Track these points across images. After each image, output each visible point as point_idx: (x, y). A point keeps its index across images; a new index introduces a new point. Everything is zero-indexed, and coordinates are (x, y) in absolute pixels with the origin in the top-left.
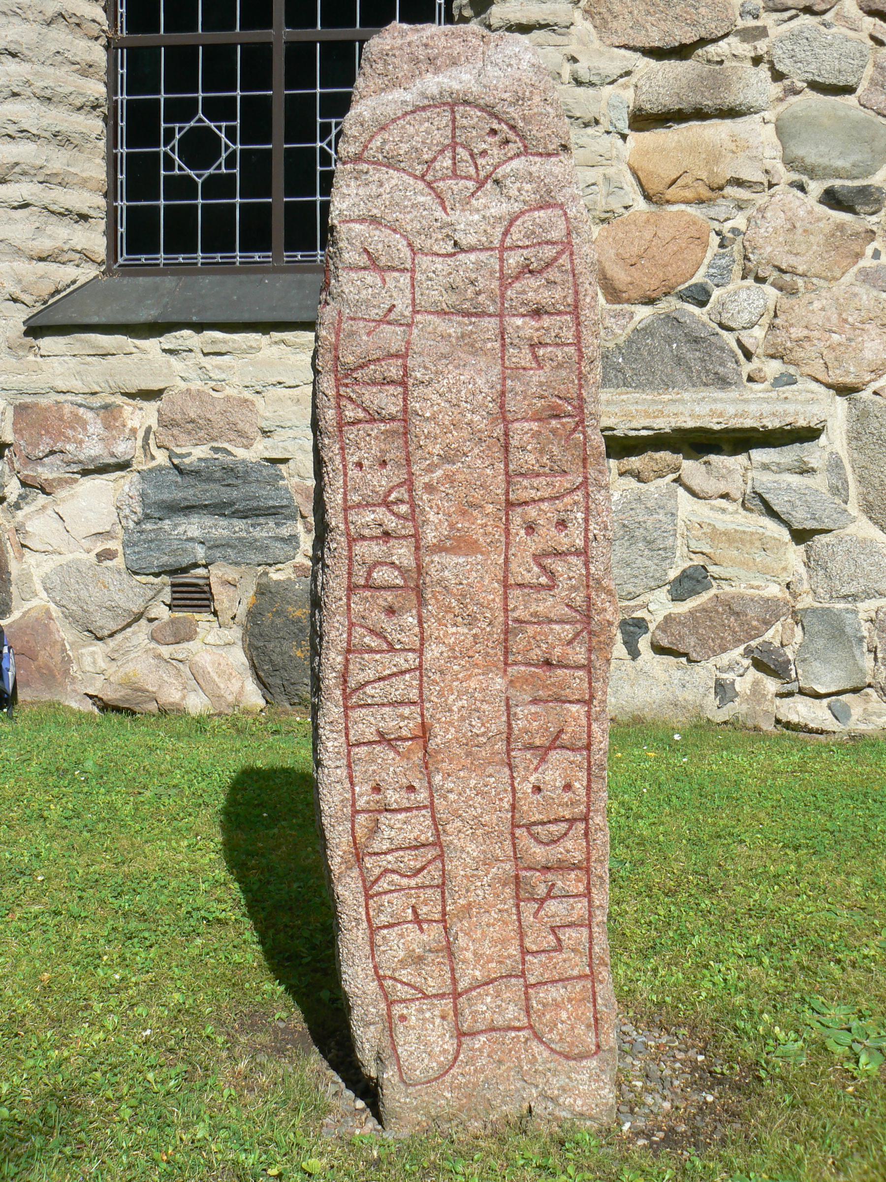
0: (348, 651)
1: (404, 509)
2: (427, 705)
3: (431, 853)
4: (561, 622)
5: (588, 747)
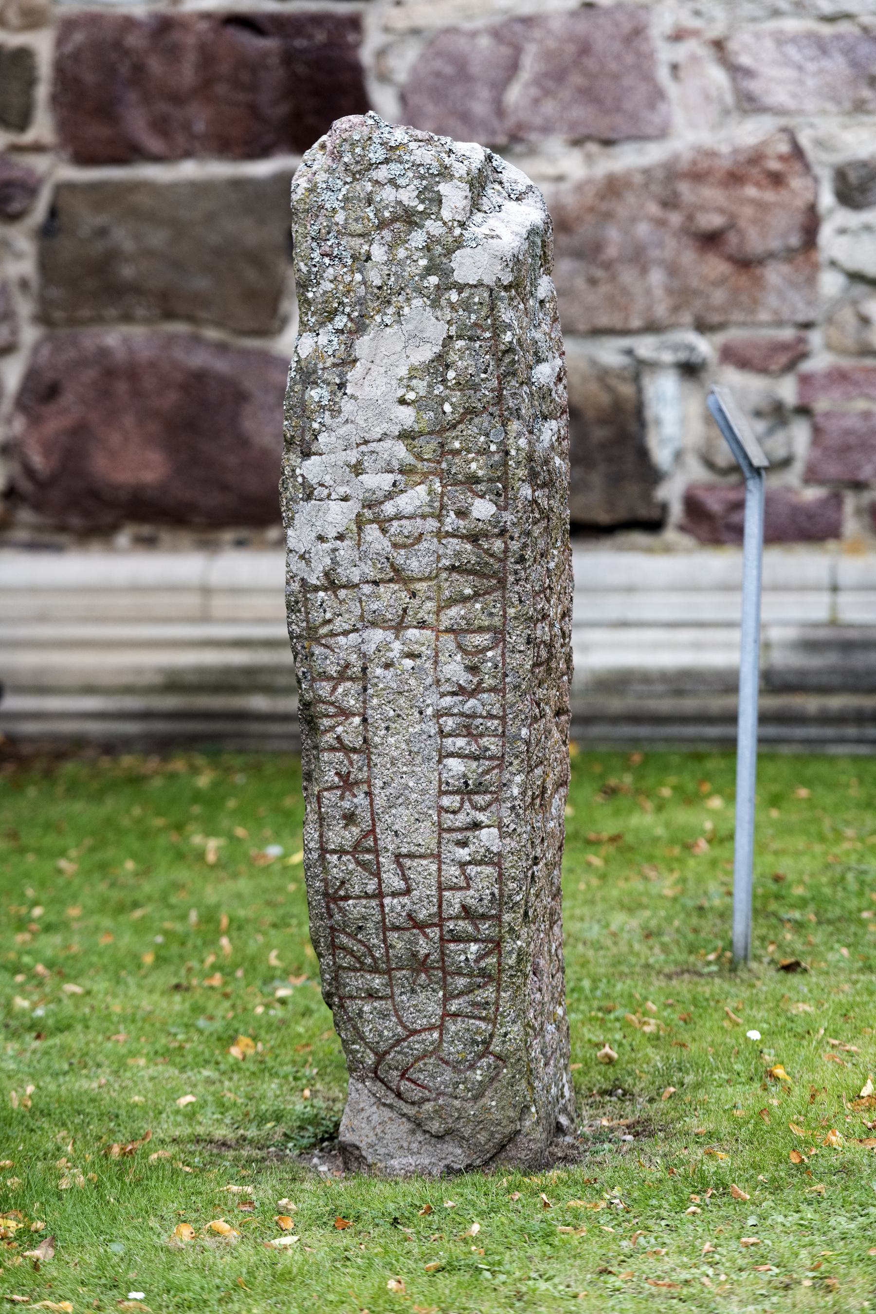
3: (496, 762)
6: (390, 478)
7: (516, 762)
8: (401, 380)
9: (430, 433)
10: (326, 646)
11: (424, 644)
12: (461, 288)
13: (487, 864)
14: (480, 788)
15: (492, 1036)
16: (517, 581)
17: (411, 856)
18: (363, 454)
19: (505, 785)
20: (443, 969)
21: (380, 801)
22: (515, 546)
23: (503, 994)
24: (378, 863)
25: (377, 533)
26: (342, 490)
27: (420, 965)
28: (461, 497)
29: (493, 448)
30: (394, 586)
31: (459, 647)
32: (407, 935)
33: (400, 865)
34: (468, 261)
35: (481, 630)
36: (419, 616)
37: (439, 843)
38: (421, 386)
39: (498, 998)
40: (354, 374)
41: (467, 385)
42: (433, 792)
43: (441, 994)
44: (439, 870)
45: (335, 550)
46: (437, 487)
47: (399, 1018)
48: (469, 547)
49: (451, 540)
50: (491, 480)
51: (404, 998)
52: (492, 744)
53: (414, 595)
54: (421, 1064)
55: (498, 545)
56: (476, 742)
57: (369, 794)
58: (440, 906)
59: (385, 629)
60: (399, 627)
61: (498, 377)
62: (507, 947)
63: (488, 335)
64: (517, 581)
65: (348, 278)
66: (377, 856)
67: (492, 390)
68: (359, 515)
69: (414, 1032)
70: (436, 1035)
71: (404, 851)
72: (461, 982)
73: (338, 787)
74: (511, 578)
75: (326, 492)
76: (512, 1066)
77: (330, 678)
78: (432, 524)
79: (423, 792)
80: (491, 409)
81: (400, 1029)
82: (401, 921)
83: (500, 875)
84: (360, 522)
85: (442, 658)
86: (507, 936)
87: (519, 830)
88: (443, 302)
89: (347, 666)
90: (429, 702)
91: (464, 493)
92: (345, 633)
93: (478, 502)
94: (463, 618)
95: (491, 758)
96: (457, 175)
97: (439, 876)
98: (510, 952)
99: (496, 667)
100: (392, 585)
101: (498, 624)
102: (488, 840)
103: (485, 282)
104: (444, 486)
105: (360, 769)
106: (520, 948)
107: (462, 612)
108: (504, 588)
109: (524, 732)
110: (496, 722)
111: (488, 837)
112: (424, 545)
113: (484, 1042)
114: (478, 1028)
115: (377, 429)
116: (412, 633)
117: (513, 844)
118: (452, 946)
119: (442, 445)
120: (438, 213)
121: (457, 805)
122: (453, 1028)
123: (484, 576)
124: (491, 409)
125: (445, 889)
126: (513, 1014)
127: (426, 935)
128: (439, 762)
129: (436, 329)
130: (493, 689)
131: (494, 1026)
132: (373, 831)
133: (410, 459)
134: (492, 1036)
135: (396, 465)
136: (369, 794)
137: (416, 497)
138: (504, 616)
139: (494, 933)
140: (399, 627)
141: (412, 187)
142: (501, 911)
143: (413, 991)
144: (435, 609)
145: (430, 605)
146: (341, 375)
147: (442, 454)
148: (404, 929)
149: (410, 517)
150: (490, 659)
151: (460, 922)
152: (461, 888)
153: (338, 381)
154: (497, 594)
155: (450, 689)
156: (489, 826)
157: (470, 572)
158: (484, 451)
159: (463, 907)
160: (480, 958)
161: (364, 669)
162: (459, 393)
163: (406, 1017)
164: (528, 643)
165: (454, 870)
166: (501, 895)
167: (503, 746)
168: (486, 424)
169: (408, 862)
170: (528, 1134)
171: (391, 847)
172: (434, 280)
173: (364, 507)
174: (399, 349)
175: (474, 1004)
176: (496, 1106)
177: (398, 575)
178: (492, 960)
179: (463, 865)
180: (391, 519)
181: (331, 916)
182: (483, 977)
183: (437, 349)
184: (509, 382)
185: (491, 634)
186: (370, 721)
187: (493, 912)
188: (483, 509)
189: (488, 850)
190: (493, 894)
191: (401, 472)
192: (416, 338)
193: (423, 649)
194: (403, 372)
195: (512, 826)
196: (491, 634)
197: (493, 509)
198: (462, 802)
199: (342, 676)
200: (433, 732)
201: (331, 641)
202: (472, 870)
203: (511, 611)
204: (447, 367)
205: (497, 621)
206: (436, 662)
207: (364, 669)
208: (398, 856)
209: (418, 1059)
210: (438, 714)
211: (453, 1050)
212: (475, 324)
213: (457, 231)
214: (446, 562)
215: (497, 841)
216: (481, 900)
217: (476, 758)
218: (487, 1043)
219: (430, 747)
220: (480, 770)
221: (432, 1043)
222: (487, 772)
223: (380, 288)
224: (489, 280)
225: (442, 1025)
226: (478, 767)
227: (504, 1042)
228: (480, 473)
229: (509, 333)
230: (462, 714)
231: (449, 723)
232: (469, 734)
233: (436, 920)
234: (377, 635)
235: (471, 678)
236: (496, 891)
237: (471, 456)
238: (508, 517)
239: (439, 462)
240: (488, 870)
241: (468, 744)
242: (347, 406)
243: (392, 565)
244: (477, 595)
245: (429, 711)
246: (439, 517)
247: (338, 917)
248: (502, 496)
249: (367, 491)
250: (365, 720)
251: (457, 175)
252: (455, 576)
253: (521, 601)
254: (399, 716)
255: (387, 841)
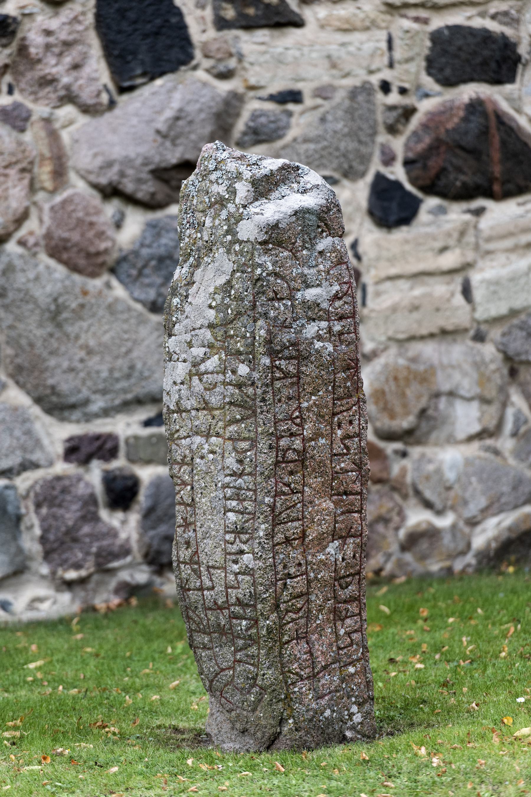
0: (276, 496)
1: (298, 421)
2: (305, 520)
3: (252, 516)
4: (352, 471)
5: (361, 535)
6: (203, 350)
7: (262, 517)
8: (210, 294)
9: (221, 325)
10: (178, 445)
11: (217, 446)
12: (241, 242)
13: (247, 574)
14: (243, 531)
15: (257, 675)
16: (262, 412)
17: (213, 567)
18: (192, 336)
19: (256, 529)
20: (232, 634)
21: (199, 535)
22: (259, 391)
23: (261, 651)
24: (200, 570)
25: (198, 381)
26: (183, 356)
27: (221, 630)
28: (234, 363)
29: (248, 335)
30: (205, 412)
31: (235, 449)
32: (215, 613)
33: (209, 572)
34: (244, 228)
35: (245, 439)
36: (216, 430)
37: (225, 561)
38: (218, 297)
39: (259, 653)
40: (192, 290)
41: (239, 299)
42: (222, 532)
43: (233, 648)
44: (226, 576)
45: (180, 390)
46: (223, 356)
47: (216, 661)
48: (237, 391)
49: (229, 387)
50: (247, 353)
51: (217, 649)
52: (249, 505)
53: (213, 418)
54: (226, 689)
55: (251, 391)
56: (242, 504)
57: (195, 530)
58: (227, 598)
59: (202, 436)
60: (208, 436)
61: (253, 294)
62: (261, 623)
63: (249, 270)
64: (262, 412)
65: (195, 236)
66: (200, 567)
67: (250, 302)
68: (190, 371)
69: (223, 670)
70: (231, 672)
71: (210, 564)
72: (241, 642)
73: (183, 526)
74: (259, 410)
75: (177, 357)
76: (270, 694)
77: (178, 463)
78: (221, 377)
79: (218, 531)
80: (249, 313)
81: (216, 667)
82: (211, 605)
83: (254, 581)
84: (191, 375)
85: (226, 455)
86: (260, 617)
87: (264, 556)
88: (232, 251)
89: (185, 457)
90: (219, 479)
91: (234, 360)
92: (185, 438)
93: (241, 365)
94: (236, 432)
95: (249, 514)
96: (245, 178)
97: (226, 580)
98: (263, 627)
99: (251, 461)
100: (204, 411)
101: (253, 436)
102: (247, 561)
103: (250, 240)
104: (226, 356)
105: (191, 516)
106: (268, 625)
107: (236, 429)
108: (256, 416)
109: (267, 500)
110: (251, 493)
111: (247, 558)
112: (217, 389)
113: (253, 678)
114: (250, 670)
115: (199, 322)
116: (213, 439)
117: (261, 564)
118: (234, 621)
119: (226, 332)
120: (234, 200)
121: (232, 539)
122: (238, 669)
123: (246, 408)
124: (249, 313)
125: (229, 588)
126: (267, 664)
127: (223, 613)
128: (224, 514)
129: (229, 267)
130: (250, 474)
131: (258, 669)
132: (197, 552)
133: (213, 341)
134: (257, 675)
135: (206, 342)
136: (195, 530)
137: (212, 363)
138: (256, 432)
139: (253, 614)
140: (208, 436)
141: (224, 184)
142: (256, 602)
143: (221, 646)
144: (223, 426)
145: (221, 424)
146: (187, 291)
147: (226, 338)
148: (214, 609)
149: (212, 373)
150: (249, 457)
151: (237, 608)
152: (236, 588)
153: (185, 294)
154: (253, 419)
155: (229, 472)
156: (248, 553)
157: (239, 406)
158: (244, 337)
159: (237, 599)
160: (247, 629)
161: (192, 459)
162: (235, 303)
163: (219, 661)
164: (270, 448)
165: (232, 577)
166: (255, 594)
167: (255, 507)
168: (245, 321)
169: (212, 571)
170: (285, 736)
171: (205, 562)
172: (229, 238)
173: (192, 366)
174: (212, 276)
175: (248, 656)
176: (263, 716)
177: (206, 406)
178: (254, 631)
179: (236, 574)
180: (204, 374)
181: (185, 600)
182: (251, 640)
183: (228, 277)
184: (260, 297)
185: (250, 442)
186: (195, 489)
187: (252, 603)
188: (243, 370)
189: (247, 566)
190: (250, 592)
191: (209, 347)
192: (219, 271)
193: (218, 448)
194: (212, 290)
195: (260, 554)
196: (250, 442)
197: (248, 370)
198: (235, 539)
199: (183, 463)
200: (221, 496)
201: (179, 442)
202: (240, 577)
203: (260, 429)
204: (232, 287)
205: (252, 435)
206: (223, 457)
207: (192, 459)
208: (208, 567)
209: (226, 685)
210: (224, 487)
211: (239, 681)
212: (244, 264)
213: (241, 210)
214: (227, 400)
215: (252, 561)
216: (245, 595)
217: (242, 513)
218: (254, 679)
219: (219, 505)
220: (243, 520)
221: (230, 676)
222: (246, 521)
223: (207, 242)
224: (252, 239)
225: (234, 667)
226: (242, 518)
227: (263, 679)
228: (242, 349)
229: (259, 269)
230: (235, 487)
231: (229, 492)
232: (238, 499)
233: (226, 605)
234: (198, 440)
235: (239, 466)
236: (252, 591)
237: (238, 339)
238: (256, 375)
239: (224, 342)
240: (248, 578)
241: (238, 504)
242: (188, 309)
243: (204, 400)
244: (243, 419)
245: (220, 485)
246: (224, 373)
247: (187, 601)
248: (252, 363)
249: (193, 357)
250: (192, 488)
251: (245, 178)
252: (233, 408)
253: (264, 424)
254: (206, 486)
255: (203, 558)
